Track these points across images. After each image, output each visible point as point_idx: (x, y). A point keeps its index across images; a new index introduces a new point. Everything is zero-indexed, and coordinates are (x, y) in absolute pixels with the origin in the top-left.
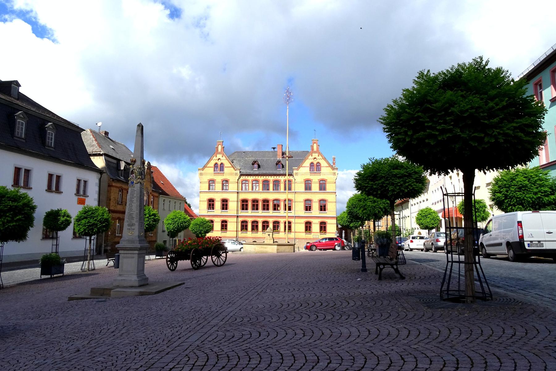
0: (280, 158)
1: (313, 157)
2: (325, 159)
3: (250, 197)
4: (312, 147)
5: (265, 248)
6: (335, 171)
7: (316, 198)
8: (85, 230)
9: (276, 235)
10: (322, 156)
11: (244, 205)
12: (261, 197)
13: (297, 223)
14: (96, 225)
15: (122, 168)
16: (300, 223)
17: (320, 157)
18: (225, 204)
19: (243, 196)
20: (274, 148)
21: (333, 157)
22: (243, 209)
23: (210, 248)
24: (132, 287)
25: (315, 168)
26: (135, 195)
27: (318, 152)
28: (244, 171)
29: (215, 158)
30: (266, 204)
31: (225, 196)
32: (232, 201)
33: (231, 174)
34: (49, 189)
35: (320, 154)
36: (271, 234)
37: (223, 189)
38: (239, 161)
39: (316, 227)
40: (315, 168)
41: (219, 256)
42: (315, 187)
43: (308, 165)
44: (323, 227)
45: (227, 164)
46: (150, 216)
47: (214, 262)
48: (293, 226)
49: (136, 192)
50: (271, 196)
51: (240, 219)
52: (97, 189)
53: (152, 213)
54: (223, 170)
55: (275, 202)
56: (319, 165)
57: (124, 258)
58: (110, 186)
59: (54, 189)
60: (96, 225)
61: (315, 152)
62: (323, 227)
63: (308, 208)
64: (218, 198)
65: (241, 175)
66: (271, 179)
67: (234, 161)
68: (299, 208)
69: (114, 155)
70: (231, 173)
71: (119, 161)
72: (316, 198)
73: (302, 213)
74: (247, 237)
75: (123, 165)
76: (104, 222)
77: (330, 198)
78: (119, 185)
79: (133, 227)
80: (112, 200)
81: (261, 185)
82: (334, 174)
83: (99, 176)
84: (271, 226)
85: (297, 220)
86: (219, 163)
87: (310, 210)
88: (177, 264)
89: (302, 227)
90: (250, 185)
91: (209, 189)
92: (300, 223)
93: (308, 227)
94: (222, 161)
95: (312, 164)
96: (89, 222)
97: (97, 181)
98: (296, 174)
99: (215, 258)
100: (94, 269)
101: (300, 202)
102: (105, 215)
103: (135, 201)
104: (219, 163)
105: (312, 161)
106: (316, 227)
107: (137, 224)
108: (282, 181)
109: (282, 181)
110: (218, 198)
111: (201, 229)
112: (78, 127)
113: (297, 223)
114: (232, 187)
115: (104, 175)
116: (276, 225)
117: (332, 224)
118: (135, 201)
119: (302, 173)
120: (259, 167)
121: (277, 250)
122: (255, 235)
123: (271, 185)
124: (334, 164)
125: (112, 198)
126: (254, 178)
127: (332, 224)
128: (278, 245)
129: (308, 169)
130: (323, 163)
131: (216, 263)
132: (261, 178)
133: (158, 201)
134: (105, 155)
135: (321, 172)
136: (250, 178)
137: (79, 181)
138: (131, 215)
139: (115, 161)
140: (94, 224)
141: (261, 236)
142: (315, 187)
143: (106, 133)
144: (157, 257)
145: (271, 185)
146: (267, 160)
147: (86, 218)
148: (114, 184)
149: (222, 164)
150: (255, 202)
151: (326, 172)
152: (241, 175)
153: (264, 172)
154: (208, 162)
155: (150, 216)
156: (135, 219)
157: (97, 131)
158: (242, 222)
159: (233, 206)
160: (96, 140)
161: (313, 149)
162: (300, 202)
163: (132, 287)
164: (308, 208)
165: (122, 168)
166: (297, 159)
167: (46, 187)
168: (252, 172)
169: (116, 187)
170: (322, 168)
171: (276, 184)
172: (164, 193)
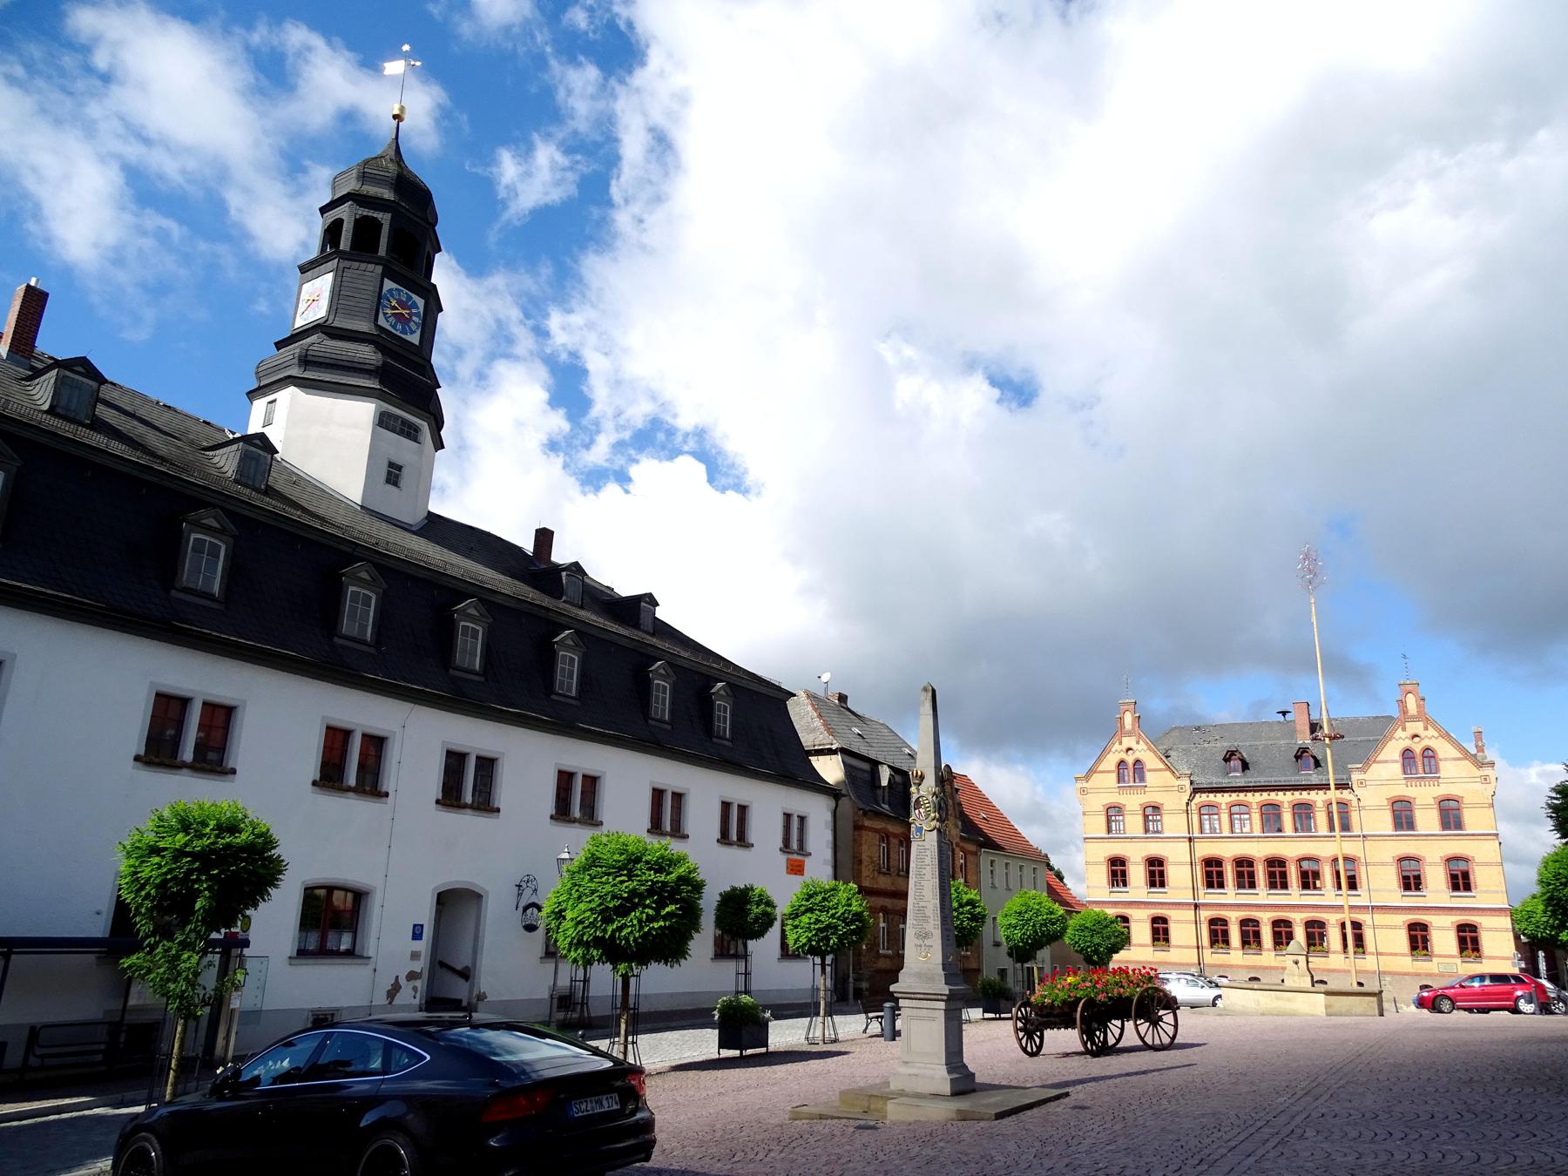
0: (1304, 739)
1: (1410, 732)
2: (1446, 736)
3: (1228, 851)
4: (1402, 703)
5: (1289, 1000)
6: (1487, 771)
7: (1434, 853)
8: (810, 940)
9: (1317, 962)
10: (1436, 729)
11: (1212, 873)
12: (1259, 850)
13: (1382, 927)
14: (836, 927)
15: (884, 783)
16: (1391, 927)
17: (1432, 732)
18: (1156, 872)
19: (1205, 849)
20: (1284, 713)
21: (1475, 729)
22: (1210, 885)
23: (1129, 999)
25: (1418, 762)
26: (928, 860)
27: (1421, 716)
28: (1203, 781)
29: (1117, 746)
30: (1245, 872)
31: (1155, 849)
32: (1176, 864)
33: (1167, 789)
34: (724, 838)
35: (1428, 722)
36: (1302, 959)
37: (1146, 830)
38: (1187, 752)
39: (1444, 940)
40: (1418, 762)
41: (1155, 1022)
42: (1428, 820)
43: (1397, 756)
44: (1468, 940)
45: (1151, 761)
46: (961, 906)
47: (1142, 1039)
48: (1368, 935)
50: (1290, 848)
51: (1205, 914)
52: (829, 836)
53: (965, 898)
54: (1142, 779)
55: (1306, 865)
56: (1429, 754)
57: (912, 1018)
59: (795, 846)
60: (836, 927)
61: (1414, 719)
62: (1468, 940)
63: (1411, 882)
64: (1136, 855)
65: (1196, 791)
66: (1286, 799)
67: (1171, 753)
68: (1381, 884)
69: (863, 751)
70: (1166, 787)
71: (875, 764)
72: (1434, 853)
73: (1397, 897)
74: (1266, 968)
75: (885, 776)
76: (852, 922)
77: (1481, 854)
78: (878, 824)
79: (927, 942)
81: (1256, 817)
82: (1485, 779)
83: (832, 803)
84: (1300, 934)
85: (1380, 918)
86: (1130, 759)
87: (1418, 889)
88: (1041, 1038)
89: (1401, 940)
90: (1225, 817)
91: (1109, 830)
92: (1391, 927)
93: (1419, 938)
94: (1138, 755)
95: (1407, 754)
96: (818, 921)
97: (828, 817)
98: (1362, 783)
99: (1144, 1027)
100: (835, 1041)
101: (1383, 864)
102: (854, 903)
104: (1130, 759)
105: (1407, 743)
106: (1444, 940)
108: (1320, 804)
109: (1320, 804)
110: (1136, 855)
111: (1097, 940)
112: (779, 689)
113: (1382, 927)
114: (1173, 823)
115: (844, 801)
116: (1316, 933)
117: (1496, 930)
119: (1380, 781)
120: (1245, 766)
121: (1327, 1007)
122: (1253, 959)
123: (1287, 818)
124: (1480, 749)
126: (1234, 797)
127: (1496, 930)
128: (1327, 993)
129: (1396, 768)
130: (1444, 749)
131: (1149, 1040)
132: (1255, 799)
133: (978, 865)
134: (844, 751)
135: (1442, 774)
136: (1223, 799)
138: (921, 909)
139: (866, 766)
140: (829, 926)
141: (1273, 964)
142: (1428, 820)
143: (843, 698)
144: (987, 1015)
145: (1287, 818)
146: (1266, 746)
147: (810, 910)
148: (867, 823)
149: (1137, 761)
150: (1244, 866)
151: (1455, 776)
152: (1196, 791)
153: (1262, 780)
154: (1099, 760)
155: (961, 906)
157: (821, 694)
158: (1213, 922)
159: (1180, 876)
160: (820, 716)
161: (1405, 711)
162: (1383, 864)
164: (1411, 882)
165: (884, 783)
166: (1360, 743)
168: (1225, 782)
169: (875, 831)
170: (1441, 764)
171: (1303, 813)
172: (990, 844)
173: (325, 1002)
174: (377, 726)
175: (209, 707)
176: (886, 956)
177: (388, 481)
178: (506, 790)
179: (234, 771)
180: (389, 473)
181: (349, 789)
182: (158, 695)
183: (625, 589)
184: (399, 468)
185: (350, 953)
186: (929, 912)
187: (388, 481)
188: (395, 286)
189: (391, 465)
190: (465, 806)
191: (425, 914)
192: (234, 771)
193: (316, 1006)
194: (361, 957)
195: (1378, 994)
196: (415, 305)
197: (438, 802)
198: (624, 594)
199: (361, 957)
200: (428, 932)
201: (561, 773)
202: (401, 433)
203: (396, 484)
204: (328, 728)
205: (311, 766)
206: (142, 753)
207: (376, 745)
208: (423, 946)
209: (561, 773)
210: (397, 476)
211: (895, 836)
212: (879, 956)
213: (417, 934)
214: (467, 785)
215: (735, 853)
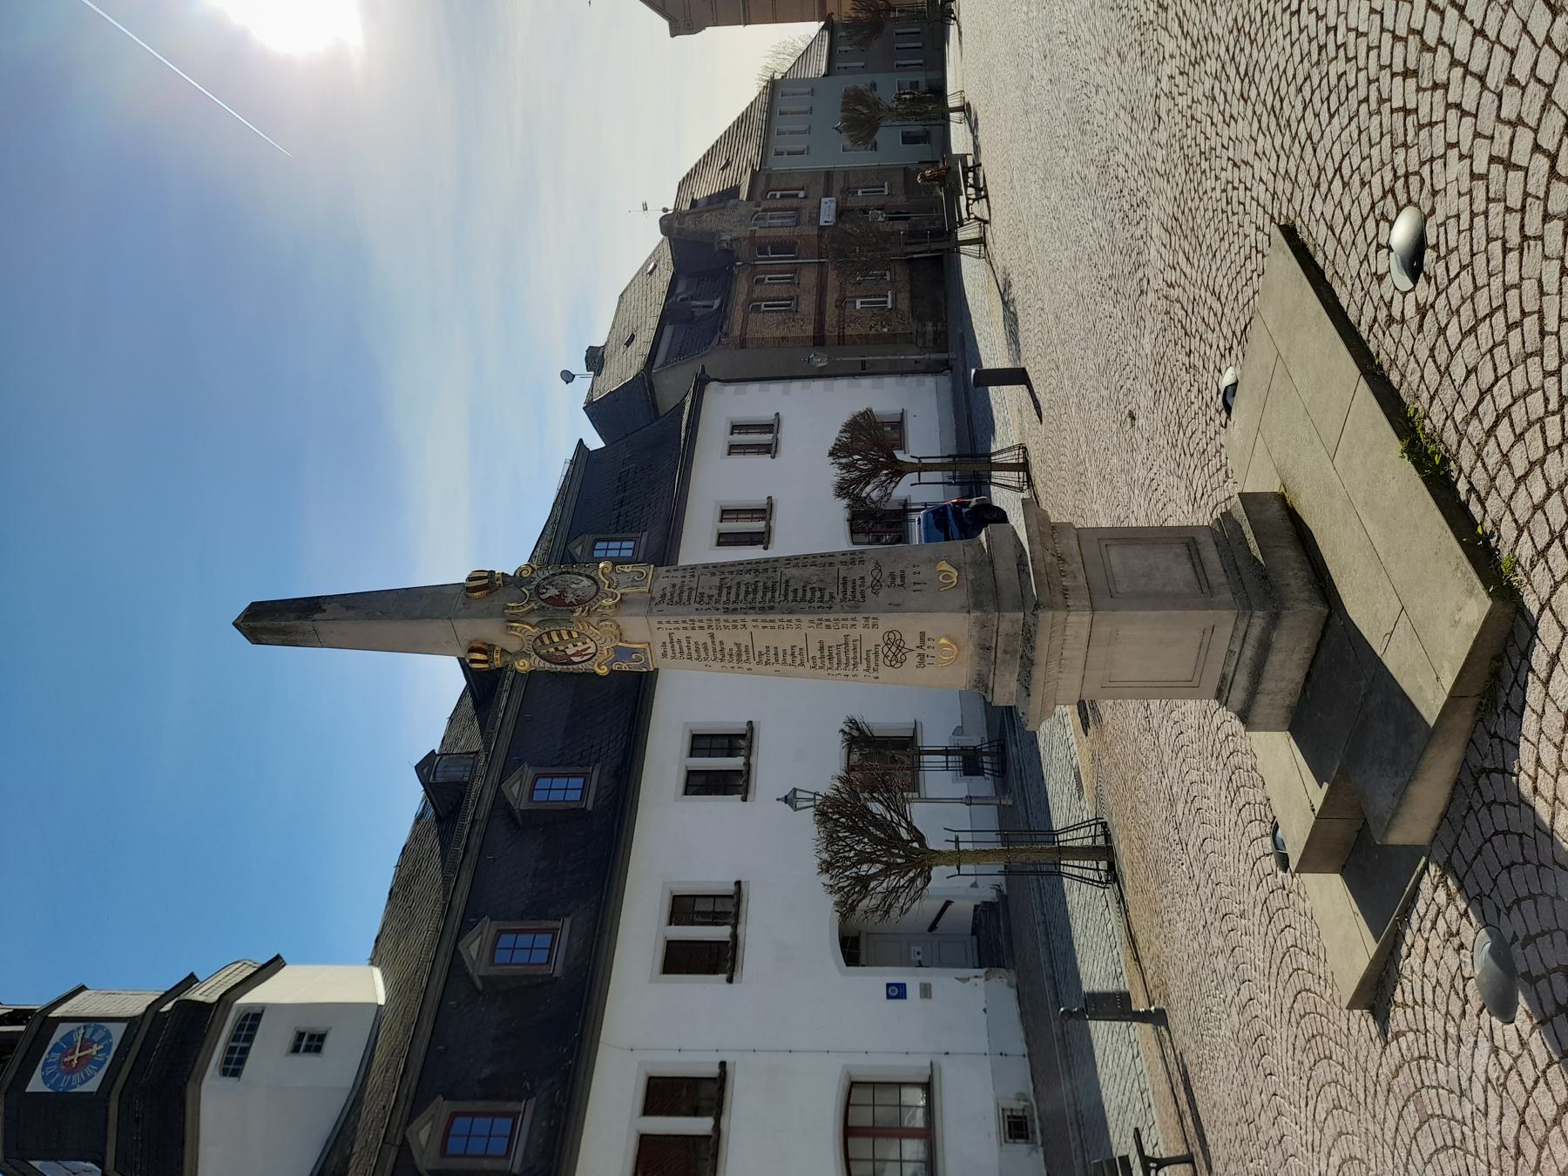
24: (1265, 647)
26: (700, 637)
34: (769, 449)
49: (680, 635)
52: (754, 388)
58: (743, 344)
59: (767, 438)
78: (737, 315)
79: (911, 641)
80: (785, 333)
83: (713, 386)
97: (731, 389)
103: (742, 637)
107: (887, 622)
112: (573, 463)
118: (742, 637)
125: (778, 334)
133: (782, 174)
137: (733, 449)
148: (737, 332)
156: (854, 634)
163: (1265, 647)
167: (731, 803)
169: (745, 321)
173: (991, 1126)
174: (634, 1094)
175: (694, 751)
176: (894, 301)
177: (318, 1049)
178: (710, 877)
179: (738, 883)
180: (308, 1049)
181: (717, 1127)
182: (669, 942)
183: (414, 795)
184: (300, 1036)
185: (928, 1087)
186: (833, 637)
187: (318, 1049)
188: (38, 1073)
189: (296, 1049)
190: (734, 936)
191: (872, 980)
192: (750, 723)
193: (995, 1145)
194: (931, 1077)
195: (1157, 1018)
196: (68, 1038)
197: (744, 800)
198: (464, 683)
199: (931, 1077)
200: (896, 975)
201: (719, 544)
202: (250, 1039)
203: (322, 1037)
204: (686, 793)
205: (726, 805)
206: (724, 976)
207: (702, 743)
208: (912, 979)
209: (719, 544)
210: (312, 1037)
211: (750, 291)
212: (894, 308)
213: (897, 992)
214: (705, 942)
215: (786, 436)
